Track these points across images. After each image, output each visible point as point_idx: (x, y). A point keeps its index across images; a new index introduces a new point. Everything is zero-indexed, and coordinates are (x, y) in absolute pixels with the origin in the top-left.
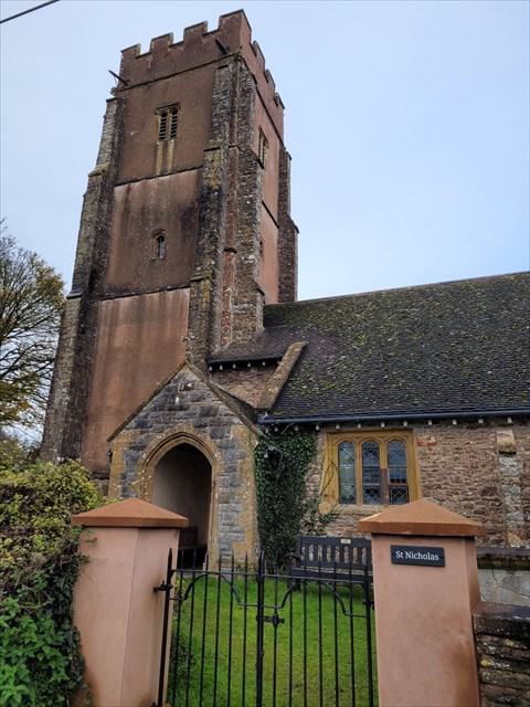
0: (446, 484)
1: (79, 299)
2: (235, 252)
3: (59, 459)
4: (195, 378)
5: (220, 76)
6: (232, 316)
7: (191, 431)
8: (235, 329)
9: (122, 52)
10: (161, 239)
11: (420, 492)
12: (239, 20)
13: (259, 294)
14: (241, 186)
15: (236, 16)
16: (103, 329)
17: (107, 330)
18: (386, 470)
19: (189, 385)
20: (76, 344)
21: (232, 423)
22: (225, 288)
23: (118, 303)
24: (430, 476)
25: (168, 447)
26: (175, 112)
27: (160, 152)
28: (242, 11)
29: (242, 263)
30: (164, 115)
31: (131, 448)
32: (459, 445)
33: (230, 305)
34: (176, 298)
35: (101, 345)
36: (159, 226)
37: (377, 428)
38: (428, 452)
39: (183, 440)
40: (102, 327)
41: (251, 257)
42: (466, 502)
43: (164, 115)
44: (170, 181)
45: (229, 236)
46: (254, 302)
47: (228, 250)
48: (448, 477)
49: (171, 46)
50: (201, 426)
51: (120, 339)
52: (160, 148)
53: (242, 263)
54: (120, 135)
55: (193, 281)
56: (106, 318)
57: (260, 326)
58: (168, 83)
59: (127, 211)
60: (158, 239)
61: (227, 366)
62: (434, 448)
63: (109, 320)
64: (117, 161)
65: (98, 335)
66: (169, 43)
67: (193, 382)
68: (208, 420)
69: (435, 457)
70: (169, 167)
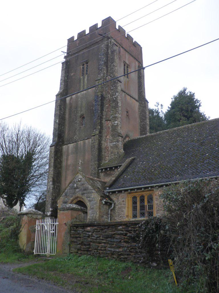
2: (110, 121)
3: (51, 209)
6: (110, 148)
7: (80, 196)
8: (111, 153)
11: (152, 210)
13: (120, 138)
16: (64, 157)
18: (146, 206)
19: (80, 180)
20: (54, 165)
23: (141, 134)
27: (82, 81)
35: (64, 164)
36: (82, 113)
37: (141, 190)
39: (79, 199)
41: (116, 122)
44: (86, 94)
47: (106, 120)
49: (85, 36)
50: (83, 194)
51: (70, 162)
55: (92, 136)
57: (122, 151)
59: (71, 107)
61: (106, 169)
63: (66, 153)
67: (81, 179)
68: (85, 192)
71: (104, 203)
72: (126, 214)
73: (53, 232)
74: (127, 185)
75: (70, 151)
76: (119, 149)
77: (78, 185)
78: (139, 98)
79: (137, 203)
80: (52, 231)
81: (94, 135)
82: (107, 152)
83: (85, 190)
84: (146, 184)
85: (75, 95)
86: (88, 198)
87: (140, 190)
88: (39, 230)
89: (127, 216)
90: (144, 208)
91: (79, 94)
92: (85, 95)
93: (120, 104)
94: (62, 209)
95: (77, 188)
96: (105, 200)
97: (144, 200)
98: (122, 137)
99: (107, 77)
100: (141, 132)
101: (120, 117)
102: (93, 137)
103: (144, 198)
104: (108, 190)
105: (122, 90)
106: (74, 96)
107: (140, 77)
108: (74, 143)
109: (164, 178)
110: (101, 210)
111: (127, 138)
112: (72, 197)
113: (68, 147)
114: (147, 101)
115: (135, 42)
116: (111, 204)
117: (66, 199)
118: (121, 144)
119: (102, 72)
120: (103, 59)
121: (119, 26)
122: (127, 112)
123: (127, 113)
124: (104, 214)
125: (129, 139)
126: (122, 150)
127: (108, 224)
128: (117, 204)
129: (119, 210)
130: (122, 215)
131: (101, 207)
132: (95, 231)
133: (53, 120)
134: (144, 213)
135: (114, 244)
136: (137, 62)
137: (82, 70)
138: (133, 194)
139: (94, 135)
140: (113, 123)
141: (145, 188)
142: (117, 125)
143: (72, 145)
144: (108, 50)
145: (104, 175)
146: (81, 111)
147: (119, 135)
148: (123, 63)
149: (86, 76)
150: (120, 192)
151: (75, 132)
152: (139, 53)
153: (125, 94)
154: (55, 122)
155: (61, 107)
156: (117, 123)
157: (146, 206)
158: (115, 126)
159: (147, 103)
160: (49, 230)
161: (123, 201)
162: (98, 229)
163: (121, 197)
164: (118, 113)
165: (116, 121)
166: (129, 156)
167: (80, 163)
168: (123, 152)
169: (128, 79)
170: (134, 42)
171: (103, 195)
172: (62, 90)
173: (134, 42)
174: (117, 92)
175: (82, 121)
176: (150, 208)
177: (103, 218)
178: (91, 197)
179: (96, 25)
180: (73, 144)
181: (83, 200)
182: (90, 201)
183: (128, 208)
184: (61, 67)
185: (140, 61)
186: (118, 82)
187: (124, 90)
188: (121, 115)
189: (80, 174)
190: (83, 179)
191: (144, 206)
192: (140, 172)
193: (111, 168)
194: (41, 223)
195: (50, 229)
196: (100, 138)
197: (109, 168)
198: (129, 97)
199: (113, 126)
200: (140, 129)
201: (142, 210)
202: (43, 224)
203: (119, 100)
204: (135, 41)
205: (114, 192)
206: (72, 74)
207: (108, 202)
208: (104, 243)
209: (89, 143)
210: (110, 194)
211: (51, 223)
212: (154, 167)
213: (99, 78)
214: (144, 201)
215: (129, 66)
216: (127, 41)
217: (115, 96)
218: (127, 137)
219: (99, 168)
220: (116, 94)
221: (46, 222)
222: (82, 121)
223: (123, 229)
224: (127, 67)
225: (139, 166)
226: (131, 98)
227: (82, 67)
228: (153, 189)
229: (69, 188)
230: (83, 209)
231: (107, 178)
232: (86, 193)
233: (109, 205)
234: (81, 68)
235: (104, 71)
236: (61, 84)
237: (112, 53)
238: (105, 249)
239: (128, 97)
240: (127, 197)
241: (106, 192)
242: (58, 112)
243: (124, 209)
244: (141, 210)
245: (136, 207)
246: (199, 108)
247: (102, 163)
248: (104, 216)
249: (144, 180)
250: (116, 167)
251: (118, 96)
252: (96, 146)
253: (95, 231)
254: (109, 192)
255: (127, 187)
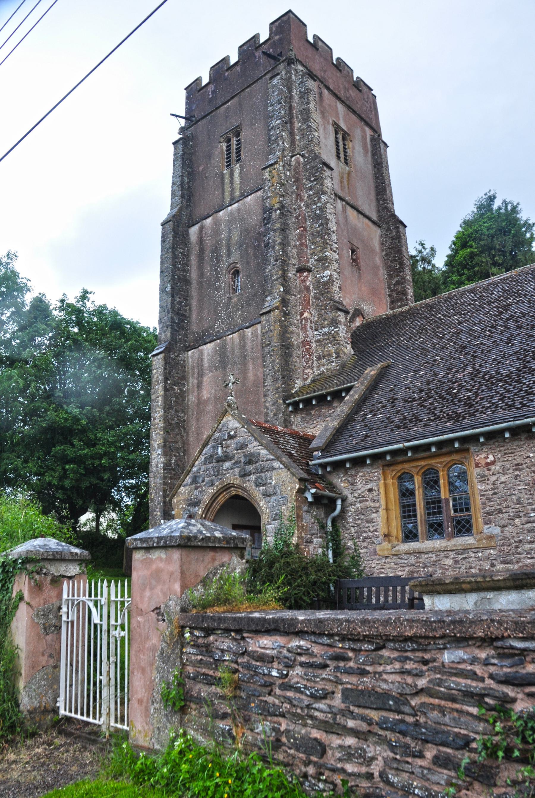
0: (508, 507)
1: (162, 356)
2: (309, 270)
4: (237, 425)
5: (274, 86)
7: (237, 482)
8: (319, 358)
9: (185, 89)
10: (237, 273)
11: (466, 513)
12: (288, 22)
14: (309, 196)
15: (285, 18)
16: (193, 381)
17: (195, 381)
19: (232, 433)
21: (273, 469)
22: (302, 314)
24: (490, 500)
25: (222, 499)
26: (238, 135)
27: (227, 181)
28: (290, 11)
29: (318, 282)
30: (228, 141)
31: (189, 505)
32: (519, 460)
33: (310, 332)
34: (255, 334)
36: (231, 260)
37: (427, 454)
38: (487, 473)
40: (191, 380)
41: (327, 272)
42: (529, 525)
43: (228, 141)
45: (300, 255)
46: (335, 323)
47: (300, 270)
48: (509, 499)
52: (227, 176)
53: (318, 282)
54: (189, 174)
56: (233, 350)
57: (349, 349)
58: (228, 108)
59: (202, 250)
60: (233, 274)
61: (307, 402)
62: (493, 467)
63: (196, 371)
64: (189, 200)
65: (188, 389)
66: (225, 68)
67: (236, 429)
68: (249, 468)
69: (493, 479)
70: (237, 193)
71: (310, 499)
72: (382, 529)
73: (123, 634)
74: (379, 440)
75: (206, 364)
76: (339, 344)
77: (228, 450)
78: (380, 217)
79: (417, 493)
80: (118, 628)
81: (269, 312)
82: (306, 355)
83: (250, 462)
84: (443, 433)
85: (211, 218)
86: (261, 488)
87: (424, 451)
88: (72, 622)
89: (387, 536)
90: (440, 507)
91: (221, 213)
92: (237, 215)
93: (333, 226)
94: (139, 545)
95: (226, 458)
96: (313, 491)
97: (437, 482)
98: (346, 312)
99: (293, 159)
100: (392, 302)
101: (336, 260)
102: (265, 317)
103: (438, 476)
104: (319, 458)
105: (336, 195)
106: (209, 221)
107: (379, 164)
108: (215, 340)
109: (501, 407)
110: (302, 521)
111: (358, 319)
112: (212, 485)
113: (201, 352)
114: (402, 223)
115: (360, 80)
116: (332, 502)
117: (197, 492)
118: (344, 332)
119: (278, 145)
120: (280, 112)
121: (315, 37)
122: (353, 251)
123: (352, 253)
124: (312, 535)
125: (365, 322)
126: (349, 347)
127: (373, 632)
128: (350, 498)
129: (359, 519)
130: (370, 534)
131: (304, 514)
132: (303, 659)
133: (159, 287)
134: (440, 525)
135: (421, 756)
136: (367, 129)
137: (226, 164)
138: (399, 467)
139: (269, 312)
140: (318, 276)
141: (440, 445)
142: (331, 281)
143: (210, 346)
144: (290, 91)
145: (304, 420)
146: (229, 255)
147: (338, 307)
148: (331, 126)
149: (238, 165)
150: (359, 462)
151: (215, 311)
152: (370, 107)
153: (344, 203)
154: (163, 290)
155: (177, 253)
156: (331, 276)
157: (447, 500)
158: (325, 284)
159: (401, 227)
160: (105, 627)
161: (370, 490)
162: (316, 649)
163: (362, 476)
164: (331, 249)
165: (325, 268)
166: (370, 361)
167: (230, 384)
168: (353, 352)
169: (347, 168)
170: (355, 79)
171: (305, 476)
172: (176, 210)
173: (355, 79)
174: (324, 193)
175: (234, 282)
176: (464, 507)
177: (311, 547)
178: (271, 483)
179: (256, 37)
180: (213, 344)
181: (245, 495)
182: (266, 495)
183: (387, 509)
184: (173, 153)
185: (374, 125)
186: (325, 168)
187: (340, 193)
188: (338, 254)
189: (232, 415)
190: (243, 429)
191: (439, 502)
192: (414, 400)
193: (322, 399)
194: (79, 595)
195: (113, 622)
196: (285, 318)
197: (317, 398)
198: (355, 213)
199: (318, 284)
200: (390, 296)
201: (434, 513)
202: (84, 599)
203: (331, 213)
204: (358, 78)
205: (338, 466)
206: (201, 168)
207: (323, 497)
208: (355, 733)
209: (257, 336)
210: (328, 470)
211: (113, 598)
212: (456, 382)
213: (273, 162)
214: (439, 486)
215: (349, 135)
216: (339, 74)
217: (319, 205)
218: (358, 316)
219: (287, 402)
220: (320, 198)
221: (96, 595)
222: (234, 282)
223: (478, 669)
224: (344, 139)
225: (406, 385)
226: (361, 216)
227: (224, 145)
228: (466, 446)
229: (202, 458)
230: (234, 538)
231: (312, 426)
232: (254, 473)
233: (325, 505)
234: (222, 149)
235: (283, 143)
236: (173, 195)
237: (300, 98)
238: (364, 770)
239: (352, 213)
240: (382, 479)
241: (314, 465)
242: (168, 265)
243: (374, 515)
244: (429, 514)
245: (414, 505)
246: (533, 245)
247: (294, 387)
248: (315, 540)
249: (432, 421)
250: (337, 395)
251: (326, 204)
252: (275, 342)
253: (303, 659)
254: (323, 466)
255: (381, 445)
